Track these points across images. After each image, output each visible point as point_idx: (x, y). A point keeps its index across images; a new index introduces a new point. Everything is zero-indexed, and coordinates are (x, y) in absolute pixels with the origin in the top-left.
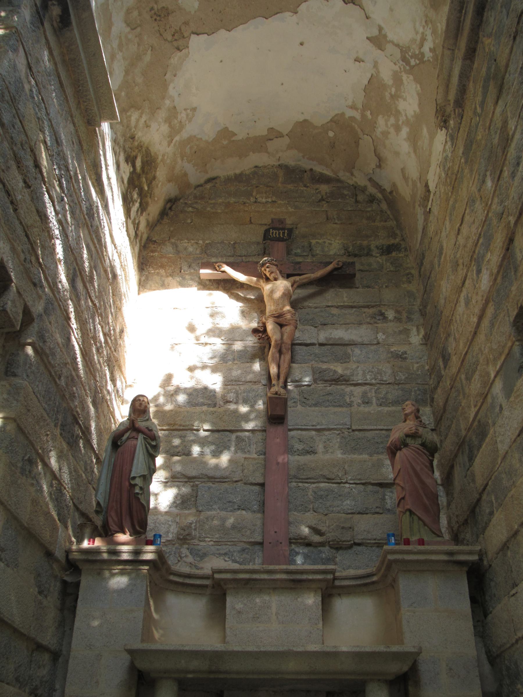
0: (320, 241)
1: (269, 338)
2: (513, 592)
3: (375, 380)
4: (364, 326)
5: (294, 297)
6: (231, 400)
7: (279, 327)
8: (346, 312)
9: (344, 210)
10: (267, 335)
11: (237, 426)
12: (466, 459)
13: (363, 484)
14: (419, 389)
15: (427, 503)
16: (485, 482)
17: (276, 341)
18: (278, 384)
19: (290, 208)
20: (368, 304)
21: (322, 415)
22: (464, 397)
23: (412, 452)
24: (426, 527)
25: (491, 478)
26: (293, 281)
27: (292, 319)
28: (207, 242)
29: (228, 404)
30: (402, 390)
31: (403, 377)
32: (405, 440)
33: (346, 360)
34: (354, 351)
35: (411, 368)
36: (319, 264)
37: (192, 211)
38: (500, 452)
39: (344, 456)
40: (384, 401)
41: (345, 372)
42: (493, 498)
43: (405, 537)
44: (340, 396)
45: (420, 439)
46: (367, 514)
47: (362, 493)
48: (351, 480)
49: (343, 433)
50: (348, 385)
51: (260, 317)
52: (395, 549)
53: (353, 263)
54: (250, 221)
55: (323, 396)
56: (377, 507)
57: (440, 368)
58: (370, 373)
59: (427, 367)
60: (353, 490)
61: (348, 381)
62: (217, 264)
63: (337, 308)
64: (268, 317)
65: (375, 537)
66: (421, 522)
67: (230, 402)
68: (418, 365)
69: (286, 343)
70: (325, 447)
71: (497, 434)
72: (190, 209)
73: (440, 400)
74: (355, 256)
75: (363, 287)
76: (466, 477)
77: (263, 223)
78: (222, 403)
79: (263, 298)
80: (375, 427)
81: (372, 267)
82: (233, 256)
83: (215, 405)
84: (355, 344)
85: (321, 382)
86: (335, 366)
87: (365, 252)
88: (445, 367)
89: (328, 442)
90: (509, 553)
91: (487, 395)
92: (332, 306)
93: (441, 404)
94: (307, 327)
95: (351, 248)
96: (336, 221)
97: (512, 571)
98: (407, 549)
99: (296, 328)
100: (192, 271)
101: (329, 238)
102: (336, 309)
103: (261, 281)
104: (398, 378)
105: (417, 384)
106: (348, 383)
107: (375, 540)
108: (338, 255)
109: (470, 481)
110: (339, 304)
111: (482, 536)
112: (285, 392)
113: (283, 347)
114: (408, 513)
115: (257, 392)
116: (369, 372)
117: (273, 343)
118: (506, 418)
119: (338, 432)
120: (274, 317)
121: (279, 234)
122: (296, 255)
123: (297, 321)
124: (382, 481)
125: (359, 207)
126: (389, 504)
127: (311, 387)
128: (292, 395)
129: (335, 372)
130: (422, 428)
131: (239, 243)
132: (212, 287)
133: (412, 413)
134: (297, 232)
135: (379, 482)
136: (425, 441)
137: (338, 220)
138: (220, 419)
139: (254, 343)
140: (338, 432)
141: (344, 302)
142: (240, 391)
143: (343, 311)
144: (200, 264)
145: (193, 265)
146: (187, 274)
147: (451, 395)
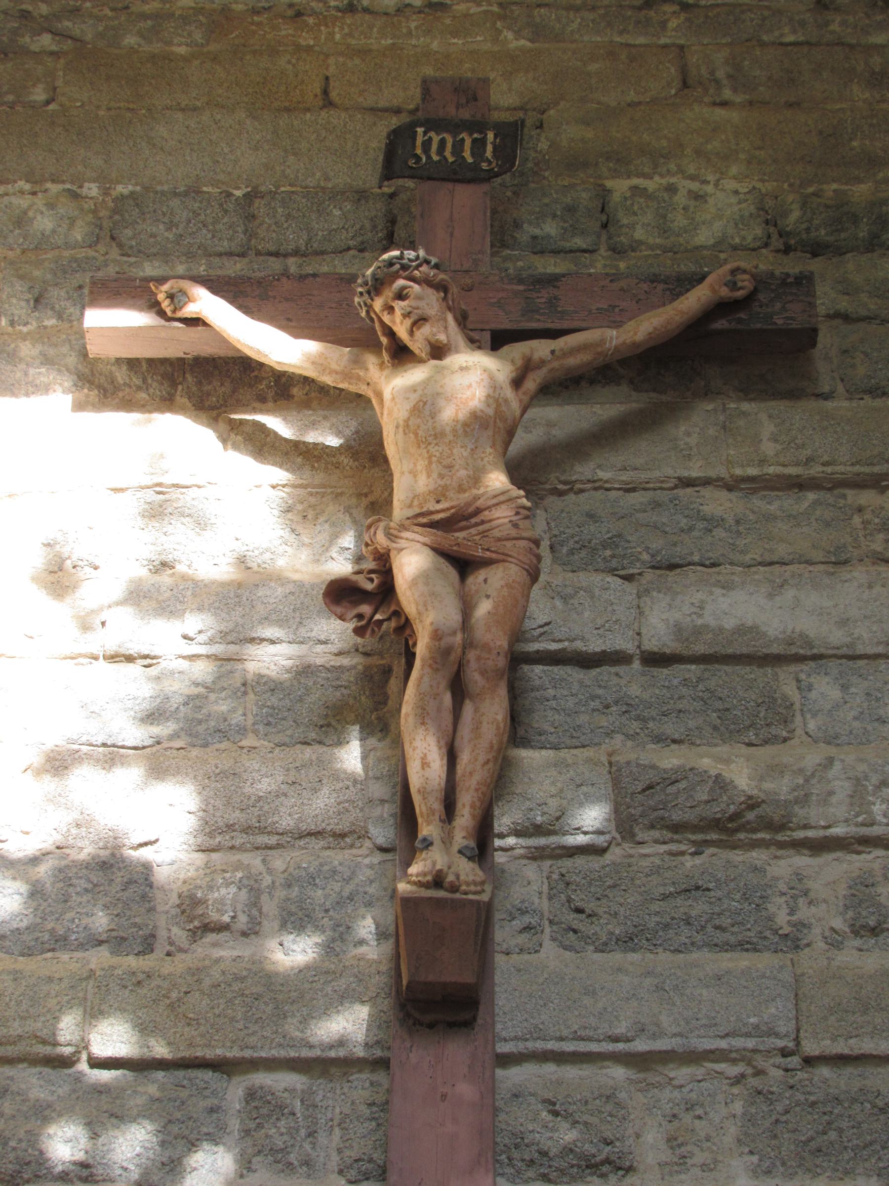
0: (650, 185)
1: (405, 627)
4: (859, 574)
5: (522, 441)
6: (226, 918)
7: (453, 573)
8: (773, 508)
9: (763, 44)
10: (398, 613)
11: (252, 1040)
17: (437, 635)
18: (447, 840)
19: (510, 35)
20: (876, 469)
21: (659, 988)
26: (519, 363)
27: (513, 533)
28: (121, 189)
29: (211, 937)
33: (774, 730)
34: (810, 688)
36: (645, 286)
37: (54, 48)
41: (768, 785)
44: (745, 898)
49: (759, 1072)
50: (781, 845)
51: (363, 531)
53: (804, 281)
54: (326, 92)
55: (665, 897)
61: (782, 827)
62: (166, 287)
63: (730, 489)
64: (403, 527)
67: (223, 928)
69: (486, 647)
70: (671, 1141)
72: (46, 40)
74: (816, 250)
75: (854, 392)
77: (382, 104)
78: (179, 934)
79: (381, 444)
82: (242, 255)
83: (148, 945)
84: (815, 658)
85: (656, 834)
86: (719, 759)
87: (863, 232)
89: (687, 1118)
92: (706, 482)
94: (584, 579)
95: (795, 215)
96: (727, 94)
99: (534, 576)
100: (51, 322)
101: (691, 170)
102: (724, 494)
103: (371, 360)
106: (780, 837)
108: (735, 248)
110: (738, 472)
112: (480, 875)
113: (473, 665)
115: (348, 881)
117: (421, 649)
119: (734, 1070)
120: (432, 525)
121: (458, 147)
122: (539, 247)
123: (537, 543)
125: (835, 27)
127: (608, 857)
128: (517, 894)
129: (721, 784)
131: (273, 194)
132: (143, 395)
134: (543, 145)
137: (735, 90)
138: (172, 1006)
139: (339, 654)
140: (734, 1070)
141: (762, 462)
142: (267, 880)
143: (757, 502)
144: (86, 291)
145: (54, 293)
146: (24, 337)
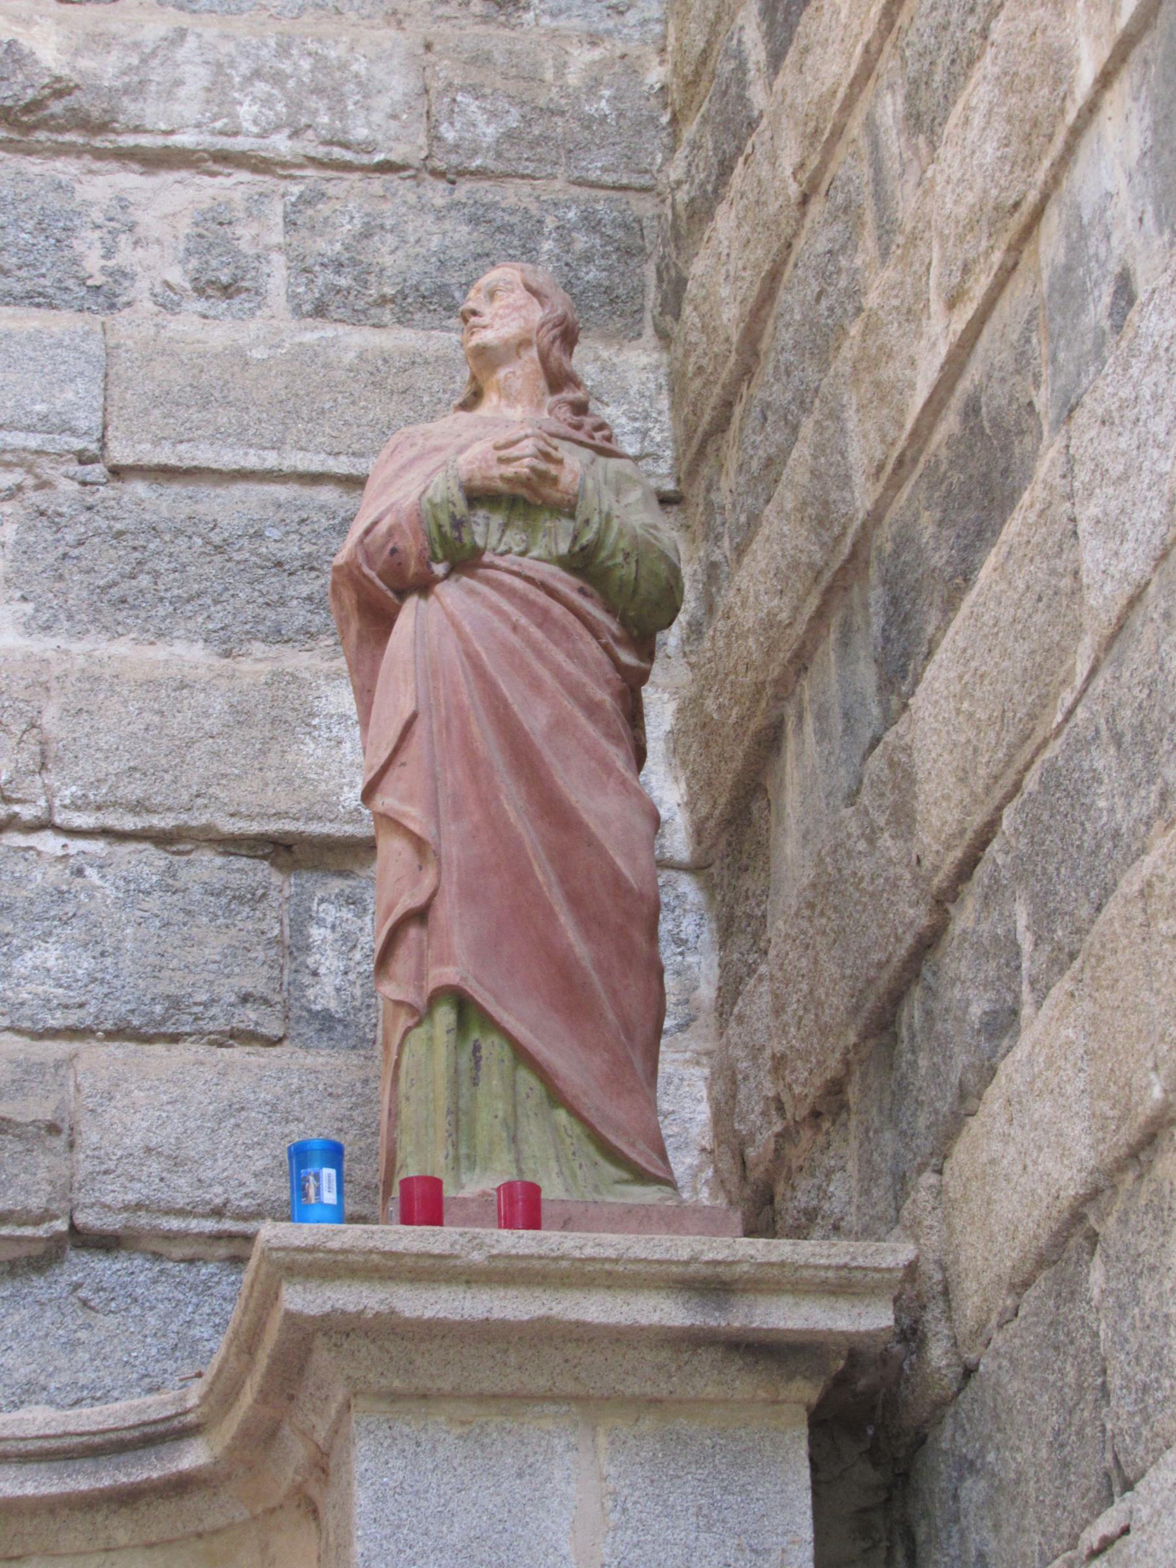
2: (1106, 1524)
3: (295, 134)
12: (867, 675)
13: (162, 839)
14: (591, 222)
15: (582, 951)
16: (978, 819)
22: (885, 253)
23: (505, 605)
24: (561, 1116)
25: (1017, 787)
30: (474, 220)
31: (489, 132)
32: (458, 524)
35: (549, 76)
38: (1093, 599)
39: (44, 645)
40: (343, 282)
41: (86, 63)
42: (1022, 920)
43: (412, 1171)
44: (41, 227)
45: (565, 526)
46: (175, 1038)
47: (152, 903)
48: (75, 806)
49: (43, 485)
50: (100, 154)
52: (335, 1244)
56: (245, 999)
57: (742, 67)
58: (261, 87)
59: (656, 74)
60: (92, 873)
61: (103, 128)
65: (216, 1195)
66: (526, 1079)
68: (597, 54)
71: (1083, 475)
73: (725, 291)
76: (852, 797)
80: (271, 460)
81: (733, 1024)
88: (776, 59)
90: (1097, 1276)
91: (1038, 214)
93: (730, 315)
97: (1104, 1390)
98: (417, 1247)
104: (449, 135)
105: (580, 183)
106: (98, 142)
107: (218, 1213)
109: (882, 821)
111: (929, 1178)
114: (445, 1016)
116: (257, 74)
118: (1154, 358)
124: (289, 826)
126: (329, 983)
130: (587, 454)
133: (524, 344)
135: (273, 827)
136: (597, 544)
147: (799, 244)
